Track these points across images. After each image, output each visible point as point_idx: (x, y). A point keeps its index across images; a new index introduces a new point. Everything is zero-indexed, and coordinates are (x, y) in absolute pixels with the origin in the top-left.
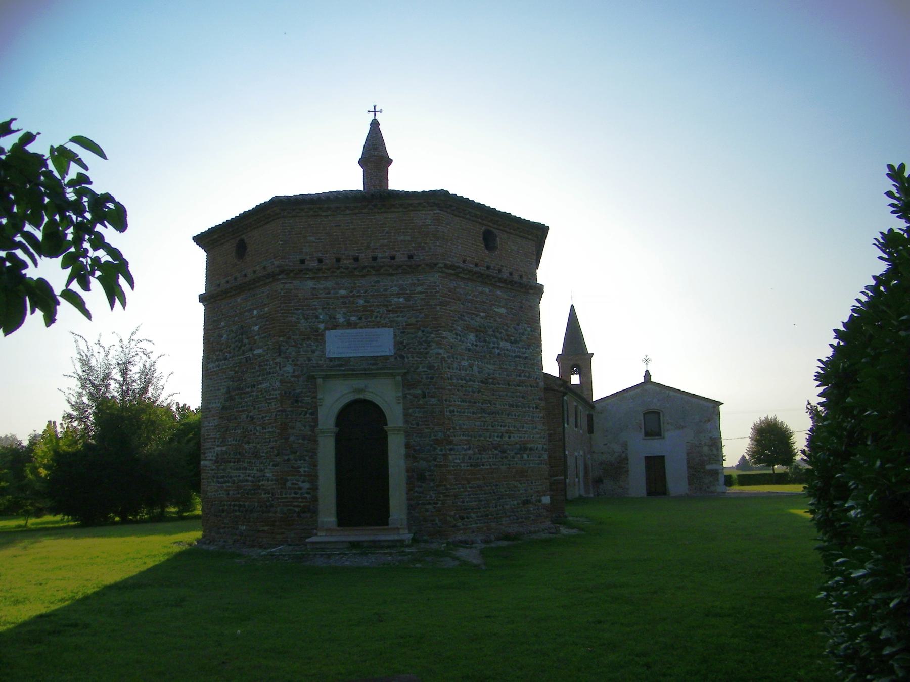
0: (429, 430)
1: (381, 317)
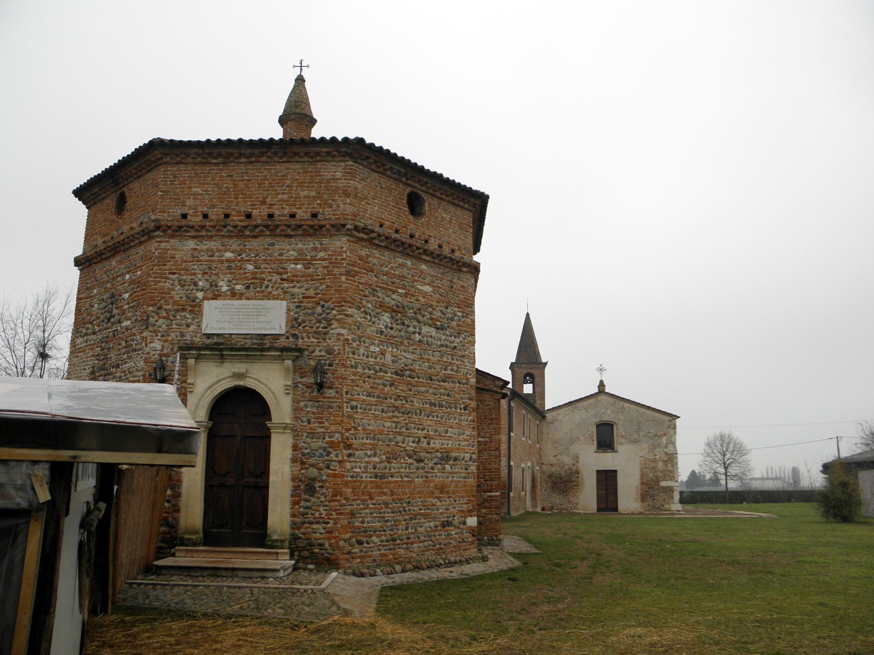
0: (323, 430)
1: (272, 287)
